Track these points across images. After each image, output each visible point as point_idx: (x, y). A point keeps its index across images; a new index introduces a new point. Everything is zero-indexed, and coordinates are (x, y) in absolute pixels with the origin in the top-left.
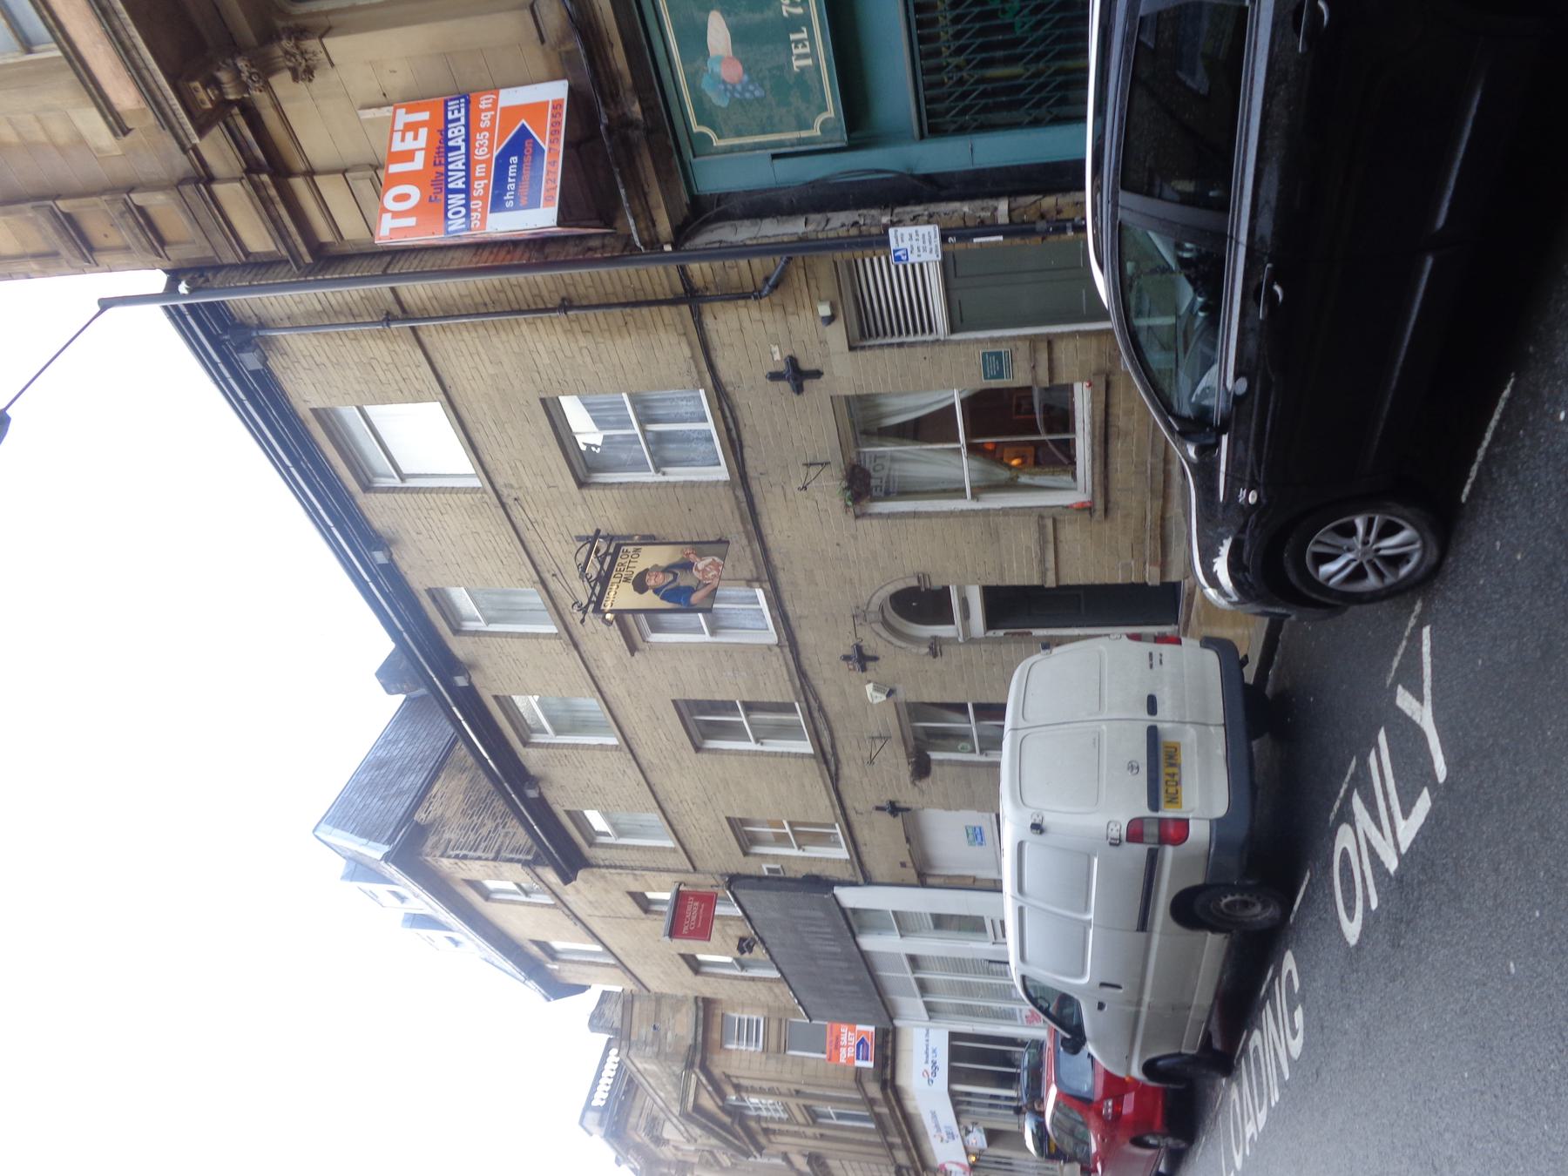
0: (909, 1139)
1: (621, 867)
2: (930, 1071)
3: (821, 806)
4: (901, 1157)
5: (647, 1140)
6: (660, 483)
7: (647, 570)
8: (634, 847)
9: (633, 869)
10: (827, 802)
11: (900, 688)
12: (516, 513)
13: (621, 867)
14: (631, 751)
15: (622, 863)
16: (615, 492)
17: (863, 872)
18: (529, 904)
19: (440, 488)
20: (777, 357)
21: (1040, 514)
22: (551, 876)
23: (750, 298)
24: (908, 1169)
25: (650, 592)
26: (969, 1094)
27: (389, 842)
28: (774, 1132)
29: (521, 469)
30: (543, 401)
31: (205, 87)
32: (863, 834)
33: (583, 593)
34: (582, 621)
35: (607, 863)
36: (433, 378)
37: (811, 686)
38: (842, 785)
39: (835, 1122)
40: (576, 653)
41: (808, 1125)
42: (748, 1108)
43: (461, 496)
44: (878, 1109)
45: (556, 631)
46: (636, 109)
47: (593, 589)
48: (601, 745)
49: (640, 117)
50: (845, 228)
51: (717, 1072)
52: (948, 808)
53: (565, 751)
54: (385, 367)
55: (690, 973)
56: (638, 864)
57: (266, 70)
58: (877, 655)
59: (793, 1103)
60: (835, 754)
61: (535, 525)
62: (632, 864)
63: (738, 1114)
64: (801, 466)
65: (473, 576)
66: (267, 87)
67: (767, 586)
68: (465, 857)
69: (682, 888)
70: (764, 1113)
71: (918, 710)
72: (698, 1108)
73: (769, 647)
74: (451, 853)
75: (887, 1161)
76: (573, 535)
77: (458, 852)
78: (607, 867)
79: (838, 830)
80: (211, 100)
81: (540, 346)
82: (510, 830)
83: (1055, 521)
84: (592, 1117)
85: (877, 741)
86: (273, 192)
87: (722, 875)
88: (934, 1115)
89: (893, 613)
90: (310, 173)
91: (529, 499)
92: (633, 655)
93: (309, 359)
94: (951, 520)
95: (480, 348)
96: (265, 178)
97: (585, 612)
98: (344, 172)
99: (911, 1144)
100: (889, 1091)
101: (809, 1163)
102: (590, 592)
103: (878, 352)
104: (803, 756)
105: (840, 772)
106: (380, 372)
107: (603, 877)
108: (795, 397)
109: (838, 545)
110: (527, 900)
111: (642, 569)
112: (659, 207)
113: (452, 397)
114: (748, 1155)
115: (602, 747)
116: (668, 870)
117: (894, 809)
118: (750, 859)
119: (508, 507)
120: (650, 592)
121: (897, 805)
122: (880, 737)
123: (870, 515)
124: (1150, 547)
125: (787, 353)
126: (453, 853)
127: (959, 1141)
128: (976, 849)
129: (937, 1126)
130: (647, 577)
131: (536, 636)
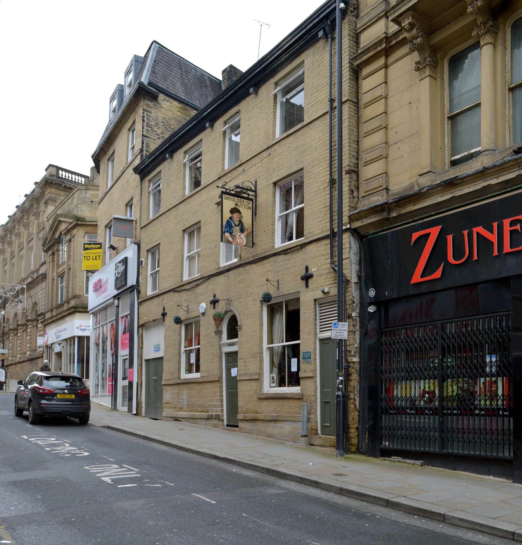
0: (55, 319)
1: (141, 195)
2: (82, 328)
3: (165, 285)
4: (48, 315)
5: (46, 198)
6: (275, 218)
7: (240, 213)
8: (149, 203)
9: (141, 200)
10: (166, 287)
12: (265, 154)
13: (141, 195)
14: (183, 201)
15: (143, 195)
16: (271, 199)
17: (143, 301)
18: (128, 150)
19: (276, 118)
20: (313, 270)
21: (260, 374)
22: (137, 162)
23: (331, 259)
24: (44, 318)
25: (231, 215)
26: (74, 344)
27: (150, 84)
28: (53, 258)
29: (280, 157)
30: (302, 169)
31: (409, 24)
32: (155, 301)
33: (231, 186)
34: (218, 187)
35: (143, 188)
36: (312, 120)
37: (205, 281)
38: (171, 293)
39: (60, 286)
40: (216, 178)
41: (57, 273)
42: (62, 246)
43: (272, 129)
44: (65, 305)
45: (226, 169)
46: (394, 214)
47: (232, 190)
48: (185, 188)
49: (392, 216)
50: (352, 298)
51: (75, 232)
52: (165, 337)
53: (182, 171)
54: (317, 97)
55: (105, 224)
56: (143, 203)
57: (420, 49)
59: (65, 266)
60: (182, 290)
61: (261, 163)
62: (143, 200)
63: (59, 241)
64: (278, 278)
65: (244, 132)
66: (412, 51)
67: (238, 264)
68: (143, 121)
69: (134, 222)
70: (61, 253)
71: (198, 323)
72: (60, 222)
73: (218, 263)
74: (145, 114)
75: (46, 309)
76: (257, 179)
77: (146, 117)
78: (141, 188)
79: (157, 291)
80: (405, 26)
81: (321, 168)
82: (157, 141)
83: (258, 379)
84: (53, 171)
85: (187, 308)
86: (379, 49)
87: (139, 241)
88: (65, 329)
89: (231, 315)
90: (386, 67)
91: (270, 160)
92: (216, 204)
93: (321, 61)
94: (259, 339)
95: (322, 141)
96: (384, 45)
97: (222, 188)
98: (386, 83)
99: (53, 319)
100: (72, 310)
101: (42, 274)
102: (231, 189)
103: (313, 310)
104: (182, 277)
106: (316, 94)
107: (138, 186)
108: (300, 277)
110: (130, 149)
111: (241, 211)
112: (362, 223)
113: (305, 128)
114: (44, 245)
115: (184, 188)
116: (141, 216)
117: (164, 315)
118: (146, 253)
119: (267, 150)
120: (231, 215)
121: (166, 316)
122: (188, 310)
123: (262, 307)
124: (249, 416)
125: (314, 274)
126: (145, 115)
127: (56, 340)
128: (152, 349)
129: (60, 331)
130: (237, 214)
131: (223, 160)
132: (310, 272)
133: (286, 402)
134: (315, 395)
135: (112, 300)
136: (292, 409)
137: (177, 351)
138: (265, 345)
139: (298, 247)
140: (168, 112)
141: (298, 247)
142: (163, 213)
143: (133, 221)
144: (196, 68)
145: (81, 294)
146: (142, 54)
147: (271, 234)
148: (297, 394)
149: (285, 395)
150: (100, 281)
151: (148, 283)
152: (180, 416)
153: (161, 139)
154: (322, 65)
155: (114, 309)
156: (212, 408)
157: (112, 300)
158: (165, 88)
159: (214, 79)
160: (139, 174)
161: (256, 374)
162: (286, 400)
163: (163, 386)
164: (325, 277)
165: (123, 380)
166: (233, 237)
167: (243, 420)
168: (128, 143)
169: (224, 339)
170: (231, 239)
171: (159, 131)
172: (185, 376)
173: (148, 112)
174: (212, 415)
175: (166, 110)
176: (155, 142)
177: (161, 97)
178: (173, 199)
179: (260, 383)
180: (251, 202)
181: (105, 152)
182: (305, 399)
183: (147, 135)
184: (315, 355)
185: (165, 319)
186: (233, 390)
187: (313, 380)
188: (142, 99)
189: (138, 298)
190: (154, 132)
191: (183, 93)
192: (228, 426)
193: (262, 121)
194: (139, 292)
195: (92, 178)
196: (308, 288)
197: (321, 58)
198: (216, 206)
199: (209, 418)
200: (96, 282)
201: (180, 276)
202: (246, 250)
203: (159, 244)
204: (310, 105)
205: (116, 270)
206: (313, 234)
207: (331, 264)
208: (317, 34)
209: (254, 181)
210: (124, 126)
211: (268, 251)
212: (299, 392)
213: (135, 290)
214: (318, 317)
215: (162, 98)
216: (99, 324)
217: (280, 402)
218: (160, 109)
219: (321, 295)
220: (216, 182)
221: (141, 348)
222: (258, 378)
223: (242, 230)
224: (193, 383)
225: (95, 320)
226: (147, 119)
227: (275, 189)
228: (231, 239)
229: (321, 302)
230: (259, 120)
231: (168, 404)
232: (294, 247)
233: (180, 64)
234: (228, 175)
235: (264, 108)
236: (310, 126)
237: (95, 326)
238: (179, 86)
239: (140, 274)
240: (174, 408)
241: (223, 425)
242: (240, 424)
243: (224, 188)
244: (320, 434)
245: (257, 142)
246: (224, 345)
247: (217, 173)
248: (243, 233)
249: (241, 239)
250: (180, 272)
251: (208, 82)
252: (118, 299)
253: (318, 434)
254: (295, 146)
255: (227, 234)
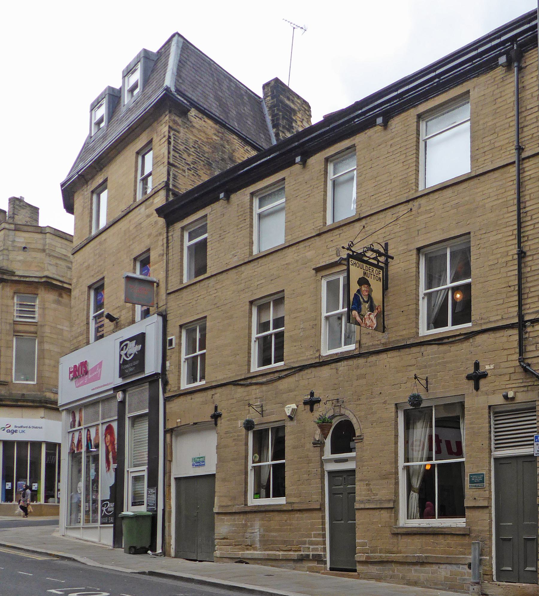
1: (168, 247)
2: (10, 429)
6: (418, 296)
7: (369, 285)
11: (294, 423)
13: (168, 247)
15: (170, 248)
18: (136, 181)
20: (487, 367)
21: (396, 501)
25: (358, 287)
30: (469, 233)
37: (294, 373)
43: (414, 176)
54: (492, 141)
56: (170, 258)
58: (314, 411)
60: (251, 384)
64: (427, 375)
67: (357, 352)
68: (169, 143)
69: (155, 284)
73: (319, 350)
77: (172, 138)
82: (187, 173)
87: (166, 311)
91: (412, 217)
93: (499, 95)
94: (394, 455)
95: (501, 201)
97: (348, 249)
105: (240, 387)
108: (465, 375)
109: (380, 393)
116: (167, 277)
120: (358, 287)
122: (262, 411)
130: (366, 286)
132: (481, 370)
133: (441, 539)
134: (490, 531)
135: (112, 392)
136: (451, 548)
137: (243, 467)
138: (401, 463)
139: (462, 337)
140: (201, 133)
141: (462, 337)
142: (212, 276)
143: (152, 283)
144: (230, 78)
145: (9, 380)
146: (154, 48)
147: (414, 316)
148: (460, 529)
149: (427, 530)
150: (84, 364)
151: (182, 372)
152: (250, 557)
153: (192, 171)
154: (499, 100)
155: (114, 406)
156: (307, 546)
157: (112, 392)
158: (196, 100)
159: (253, 95)
160: (164, 218)
161: (389, 501)
162: (441, 537)
163: (216, 516)
164: (507, 377)
165: (132, 505)
166: (362, 316)
167: (362, 563)
168: (136, 171)
169: (328, 454)
170: (358, 319)
171: (190, 160)
172: (253, 502)
173: (175, 130)
174: (308, 556)
175: (199, 131)
176: (184, 174)
177: (193, 112)
178: (231, 256)
179: (394, 513)
180: (381, 271)
181: (85, 180)
182: (473, 535)
183: (174, 162)
184: (490, 478)
185: (219, 422)
186: (343, 522)
187: (487, 511)
188: (167, 112)
189: (164, 392)
190: (183, 160)
191: (218, 109)
192: (331, 569)
193: (395, 163)
194: (166, 383)
195: (11, 213)
196: (479, 390)
197: (498, 91)
198: (314, 271)
199: (302, 559)
200: (75, 366)
201: (246, 364)
202: (370, 336)
203: (205, 317)
204: (482, 151)
205: (122, 350)
206: (487, 321)
207: (519, 362)
208: (496, 58)
209: (384, 243)
210: (128, 148)
211: (409, 339)
212: (464, 525)
213: (160, 380)
214: (493, 429)
215: (193, 114)
216: (80, 425)
217: (430, 539)
218: (191, 129)
219: (501, 400)
220: (313, 239)
221: (168, 460)
222: (392, 506)
223: (372, 308)
224: (273, 511)
225: (71, 420)
226: (174, 140)
227: (419, 257)
228: (358, 319)
229: (497, 410)
230: (390, 162)
231: (225, 540)
232: (455, 336)
233: (211, 69)
234: (335, 231)
235: (399, 146)
236: (482, 178)
237: (71, 428)
238: (213, 100)
239: (168, 358)
240: (236, 545)
241: (325, 568)
242: (359, 568)
243: (351, 250)
244: (496, 580)
245: (387, 192)
246: (329, 461)
247: (313, 227)
248: (373, 312)
249: (371, 319)
250: (246, 359)
251: (245, 98)
252: (124, 392)
253: (493, 581)
254: (456, 202)
255: (355, 313)
